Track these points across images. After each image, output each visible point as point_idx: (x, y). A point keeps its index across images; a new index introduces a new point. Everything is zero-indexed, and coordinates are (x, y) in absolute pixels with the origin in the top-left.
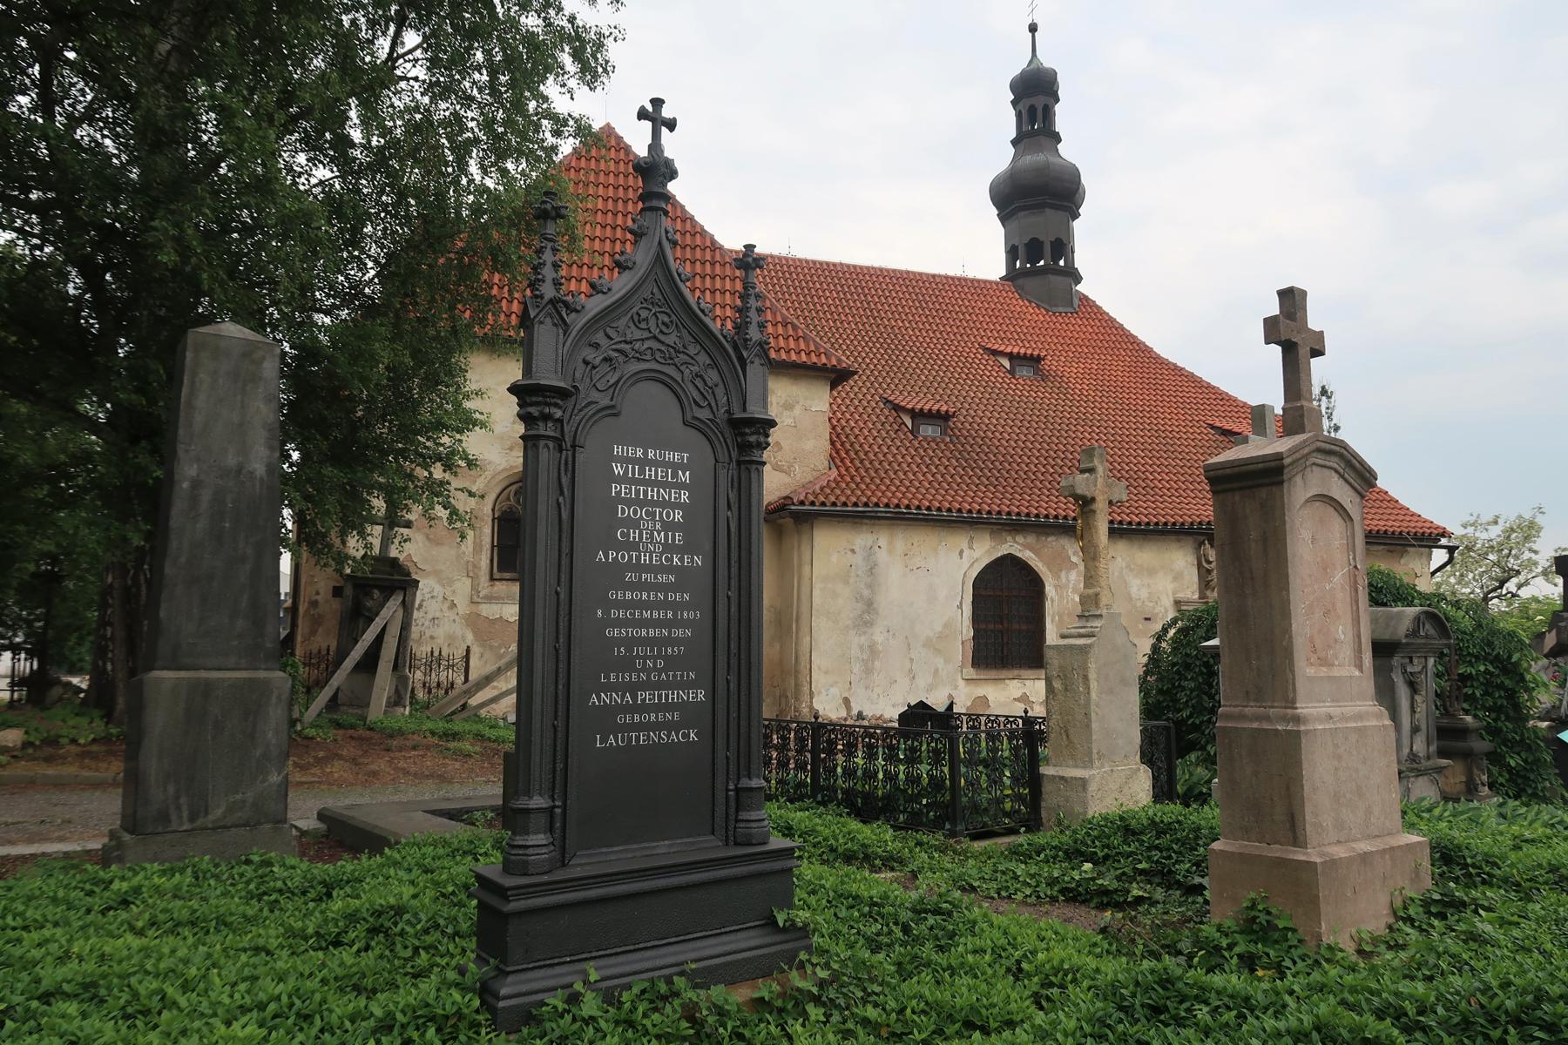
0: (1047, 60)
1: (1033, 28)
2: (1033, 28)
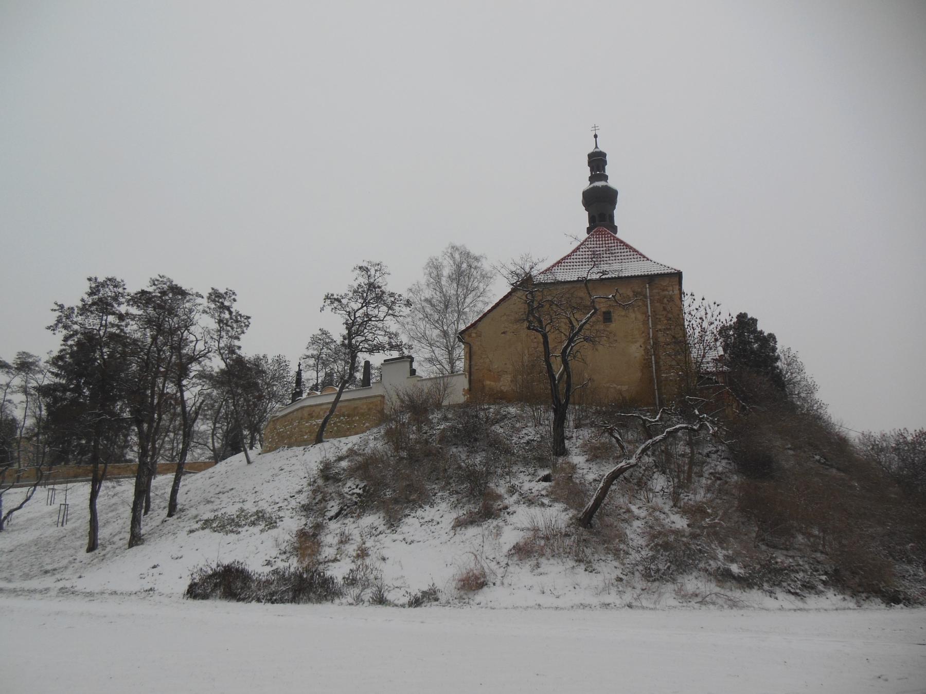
0: (602, 148)
1: (596, 136)
2: (596, 136)
